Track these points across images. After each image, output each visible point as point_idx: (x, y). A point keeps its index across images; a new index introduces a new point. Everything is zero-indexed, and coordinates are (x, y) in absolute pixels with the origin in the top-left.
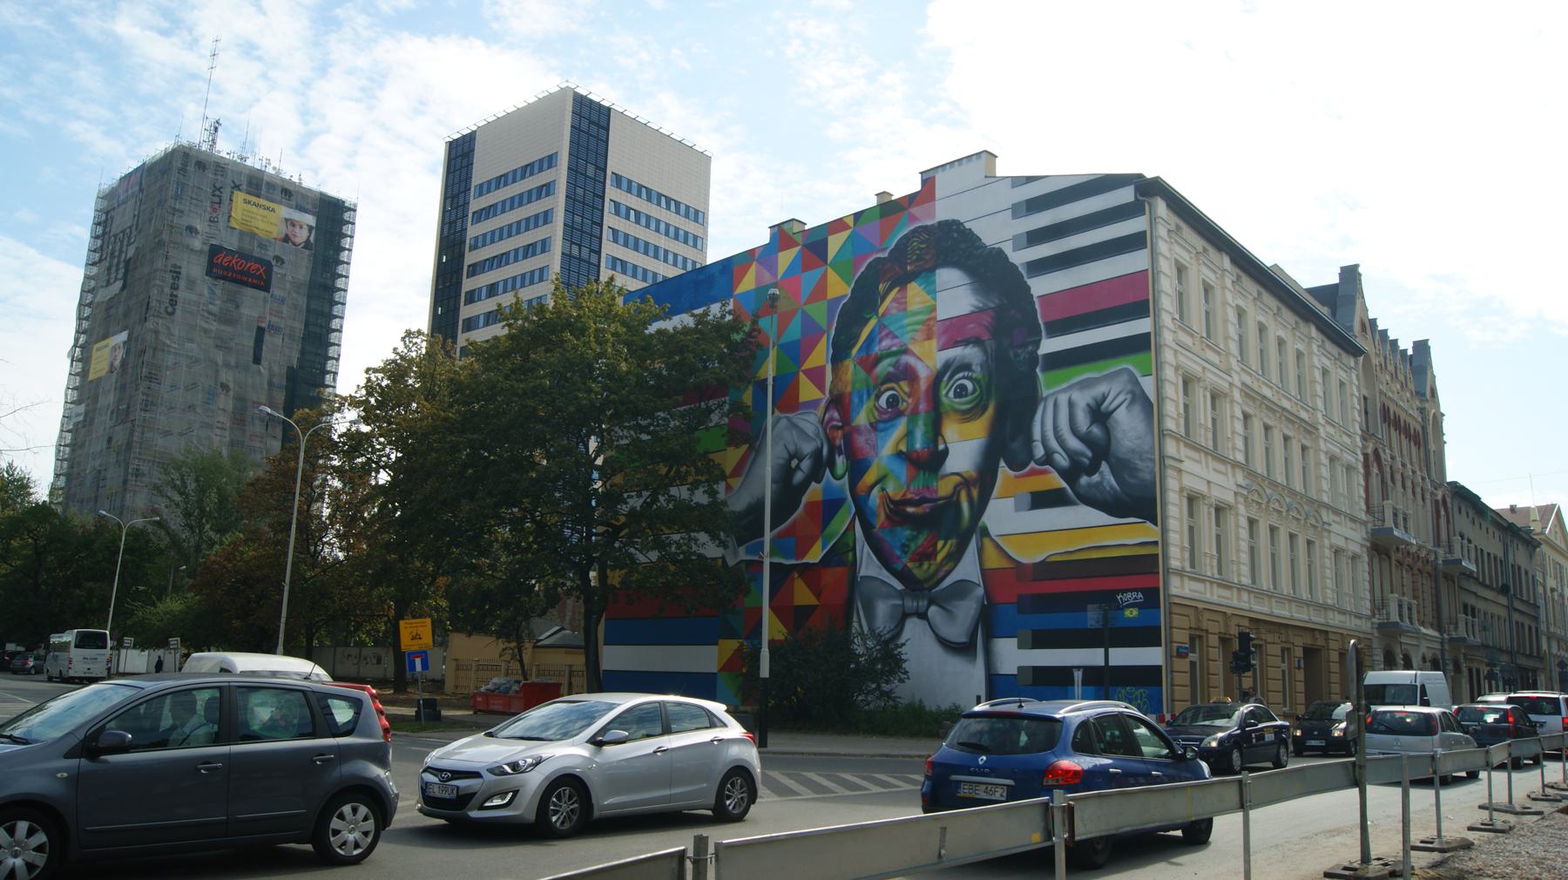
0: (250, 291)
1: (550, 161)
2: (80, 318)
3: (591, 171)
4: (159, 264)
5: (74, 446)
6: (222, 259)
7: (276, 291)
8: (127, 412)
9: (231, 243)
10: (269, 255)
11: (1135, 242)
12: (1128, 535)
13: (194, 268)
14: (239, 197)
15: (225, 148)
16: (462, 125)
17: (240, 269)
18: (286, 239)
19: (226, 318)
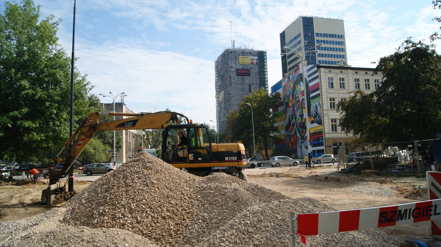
0: (246, 77)
1: (299, 35)
2: (216, 89)
3: (310, 34)
4: (227, 76)
5: (219, 116)
6: (239, 71)
7: (252, 75)
8: (226, 108)
9: (240, 67)
10: (249, 68)
11: (317, 77)
12: (320, 128)
13: (233, 75)
14: (240, 57)
15: (237, 46)
16: (281, 31)
17: (243, 73)
18: (252, 63)
19: (242, 84)
